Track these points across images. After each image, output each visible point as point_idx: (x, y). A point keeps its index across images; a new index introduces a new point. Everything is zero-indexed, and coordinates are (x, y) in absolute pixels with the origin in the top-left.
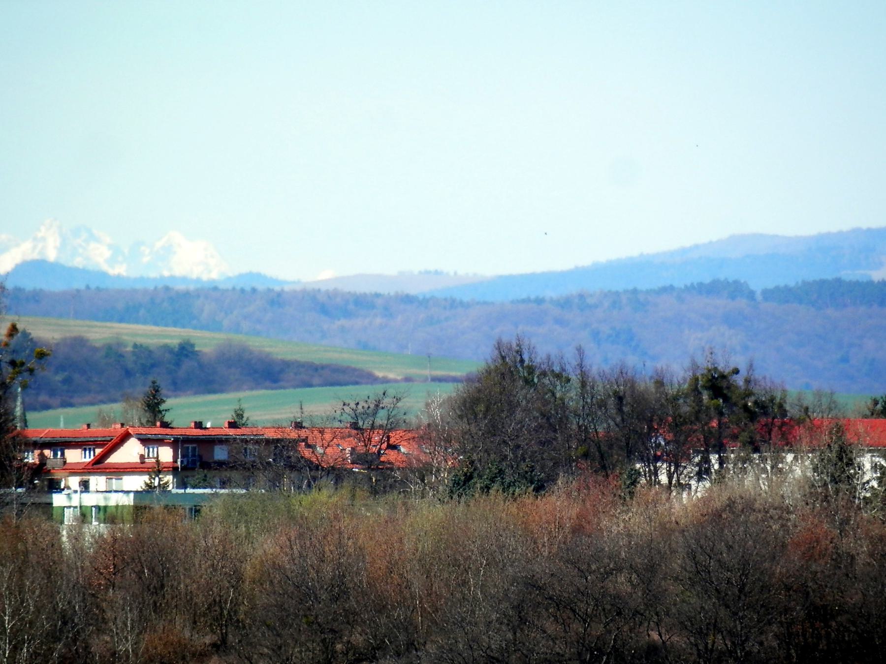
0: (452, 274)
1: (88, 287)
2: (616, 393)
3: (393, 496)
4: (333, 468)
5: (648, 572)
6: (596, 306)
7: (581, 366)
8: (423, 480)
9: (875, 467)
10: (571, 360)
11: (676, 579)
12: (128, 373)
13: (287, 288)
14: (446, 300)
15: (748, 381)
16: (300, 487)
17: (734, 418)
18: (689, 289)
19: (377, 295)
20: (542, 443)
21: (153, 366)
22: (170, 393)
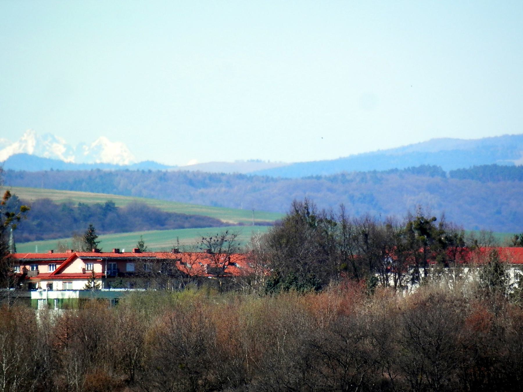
0: (267, 161)
1: (52, 170)
2: (363, 232)
3: (232, 293)
4: (197, 276)
5: (383, 338)
6: (352, 181)
7: (343, 216)
8: (250, 284)
9: (516, 276)
10: (337, 213)
11: (399, 342)
12: (76, 220)
13: (169, 170)
14: (263, 177)
15: (441, 225)
16: (177, 288)
17: (433, 247)
18: (407, 171)
19: (223, 174)
20: (320, 262)
21: (90, 216)
22: (100, 232)
